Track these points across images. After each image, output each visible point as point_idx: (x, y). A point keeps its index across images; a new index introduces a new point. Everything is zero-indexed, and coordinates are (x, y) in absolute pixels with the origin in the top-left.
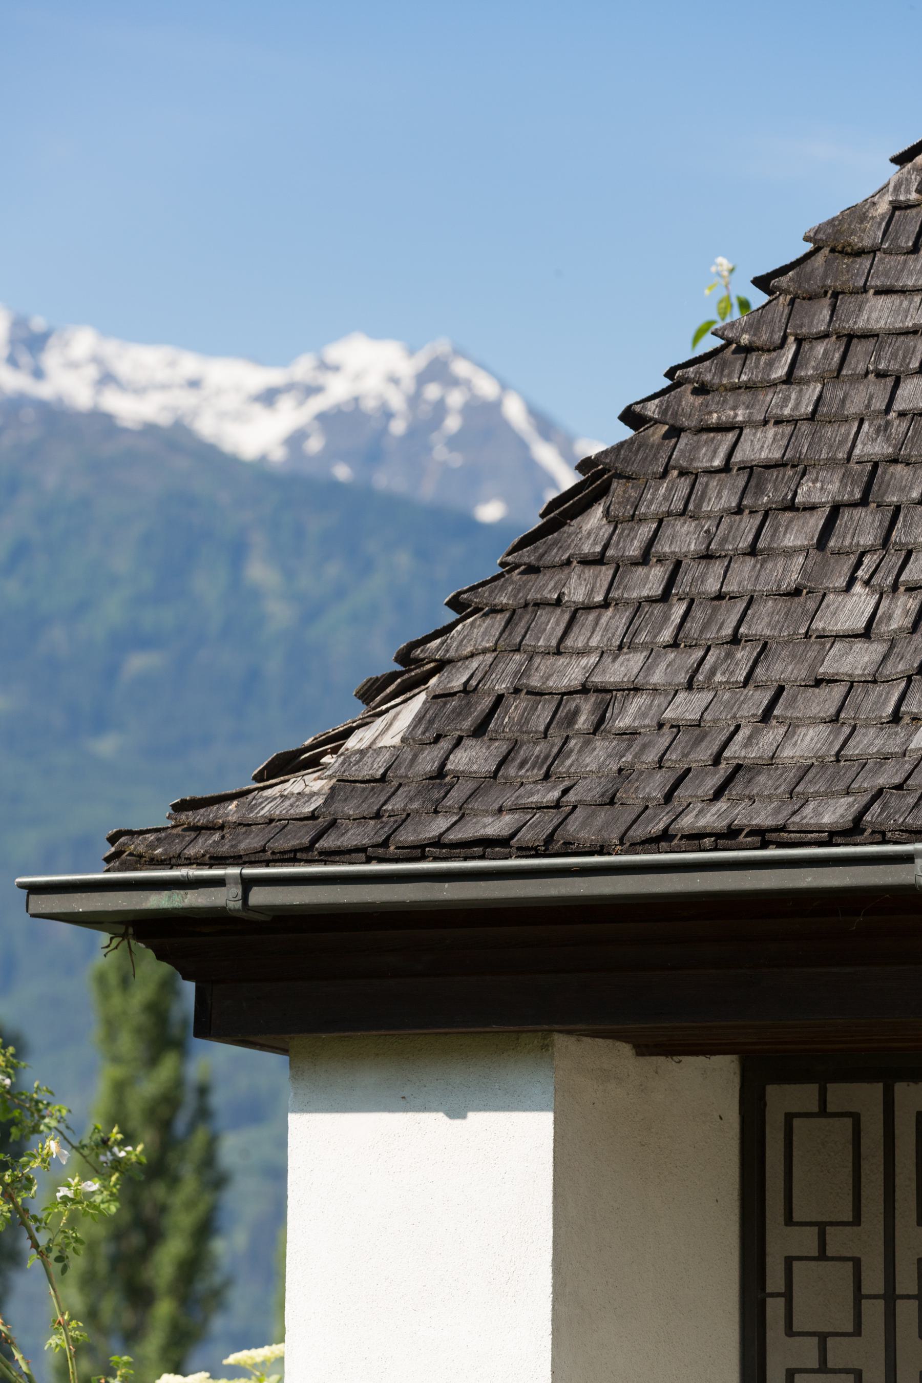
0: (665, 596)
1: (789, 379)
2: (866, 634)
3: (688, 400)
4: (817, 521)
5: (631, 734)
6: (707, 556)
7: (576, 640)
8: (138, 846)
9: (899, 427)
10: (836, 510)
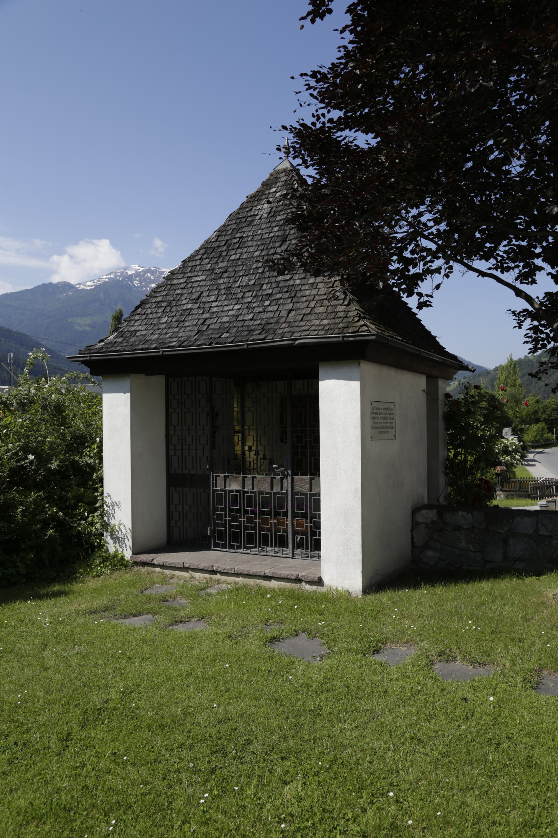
0: (145, 319)
1: (164, 290)
2: (166, 323)
3: (153, 293)
4: (163, 308)
5: (137, 336)
6: (151, 313)
7: (135, 324)
8: (81, 352)
9: (175, 296)
10: (166, 307)
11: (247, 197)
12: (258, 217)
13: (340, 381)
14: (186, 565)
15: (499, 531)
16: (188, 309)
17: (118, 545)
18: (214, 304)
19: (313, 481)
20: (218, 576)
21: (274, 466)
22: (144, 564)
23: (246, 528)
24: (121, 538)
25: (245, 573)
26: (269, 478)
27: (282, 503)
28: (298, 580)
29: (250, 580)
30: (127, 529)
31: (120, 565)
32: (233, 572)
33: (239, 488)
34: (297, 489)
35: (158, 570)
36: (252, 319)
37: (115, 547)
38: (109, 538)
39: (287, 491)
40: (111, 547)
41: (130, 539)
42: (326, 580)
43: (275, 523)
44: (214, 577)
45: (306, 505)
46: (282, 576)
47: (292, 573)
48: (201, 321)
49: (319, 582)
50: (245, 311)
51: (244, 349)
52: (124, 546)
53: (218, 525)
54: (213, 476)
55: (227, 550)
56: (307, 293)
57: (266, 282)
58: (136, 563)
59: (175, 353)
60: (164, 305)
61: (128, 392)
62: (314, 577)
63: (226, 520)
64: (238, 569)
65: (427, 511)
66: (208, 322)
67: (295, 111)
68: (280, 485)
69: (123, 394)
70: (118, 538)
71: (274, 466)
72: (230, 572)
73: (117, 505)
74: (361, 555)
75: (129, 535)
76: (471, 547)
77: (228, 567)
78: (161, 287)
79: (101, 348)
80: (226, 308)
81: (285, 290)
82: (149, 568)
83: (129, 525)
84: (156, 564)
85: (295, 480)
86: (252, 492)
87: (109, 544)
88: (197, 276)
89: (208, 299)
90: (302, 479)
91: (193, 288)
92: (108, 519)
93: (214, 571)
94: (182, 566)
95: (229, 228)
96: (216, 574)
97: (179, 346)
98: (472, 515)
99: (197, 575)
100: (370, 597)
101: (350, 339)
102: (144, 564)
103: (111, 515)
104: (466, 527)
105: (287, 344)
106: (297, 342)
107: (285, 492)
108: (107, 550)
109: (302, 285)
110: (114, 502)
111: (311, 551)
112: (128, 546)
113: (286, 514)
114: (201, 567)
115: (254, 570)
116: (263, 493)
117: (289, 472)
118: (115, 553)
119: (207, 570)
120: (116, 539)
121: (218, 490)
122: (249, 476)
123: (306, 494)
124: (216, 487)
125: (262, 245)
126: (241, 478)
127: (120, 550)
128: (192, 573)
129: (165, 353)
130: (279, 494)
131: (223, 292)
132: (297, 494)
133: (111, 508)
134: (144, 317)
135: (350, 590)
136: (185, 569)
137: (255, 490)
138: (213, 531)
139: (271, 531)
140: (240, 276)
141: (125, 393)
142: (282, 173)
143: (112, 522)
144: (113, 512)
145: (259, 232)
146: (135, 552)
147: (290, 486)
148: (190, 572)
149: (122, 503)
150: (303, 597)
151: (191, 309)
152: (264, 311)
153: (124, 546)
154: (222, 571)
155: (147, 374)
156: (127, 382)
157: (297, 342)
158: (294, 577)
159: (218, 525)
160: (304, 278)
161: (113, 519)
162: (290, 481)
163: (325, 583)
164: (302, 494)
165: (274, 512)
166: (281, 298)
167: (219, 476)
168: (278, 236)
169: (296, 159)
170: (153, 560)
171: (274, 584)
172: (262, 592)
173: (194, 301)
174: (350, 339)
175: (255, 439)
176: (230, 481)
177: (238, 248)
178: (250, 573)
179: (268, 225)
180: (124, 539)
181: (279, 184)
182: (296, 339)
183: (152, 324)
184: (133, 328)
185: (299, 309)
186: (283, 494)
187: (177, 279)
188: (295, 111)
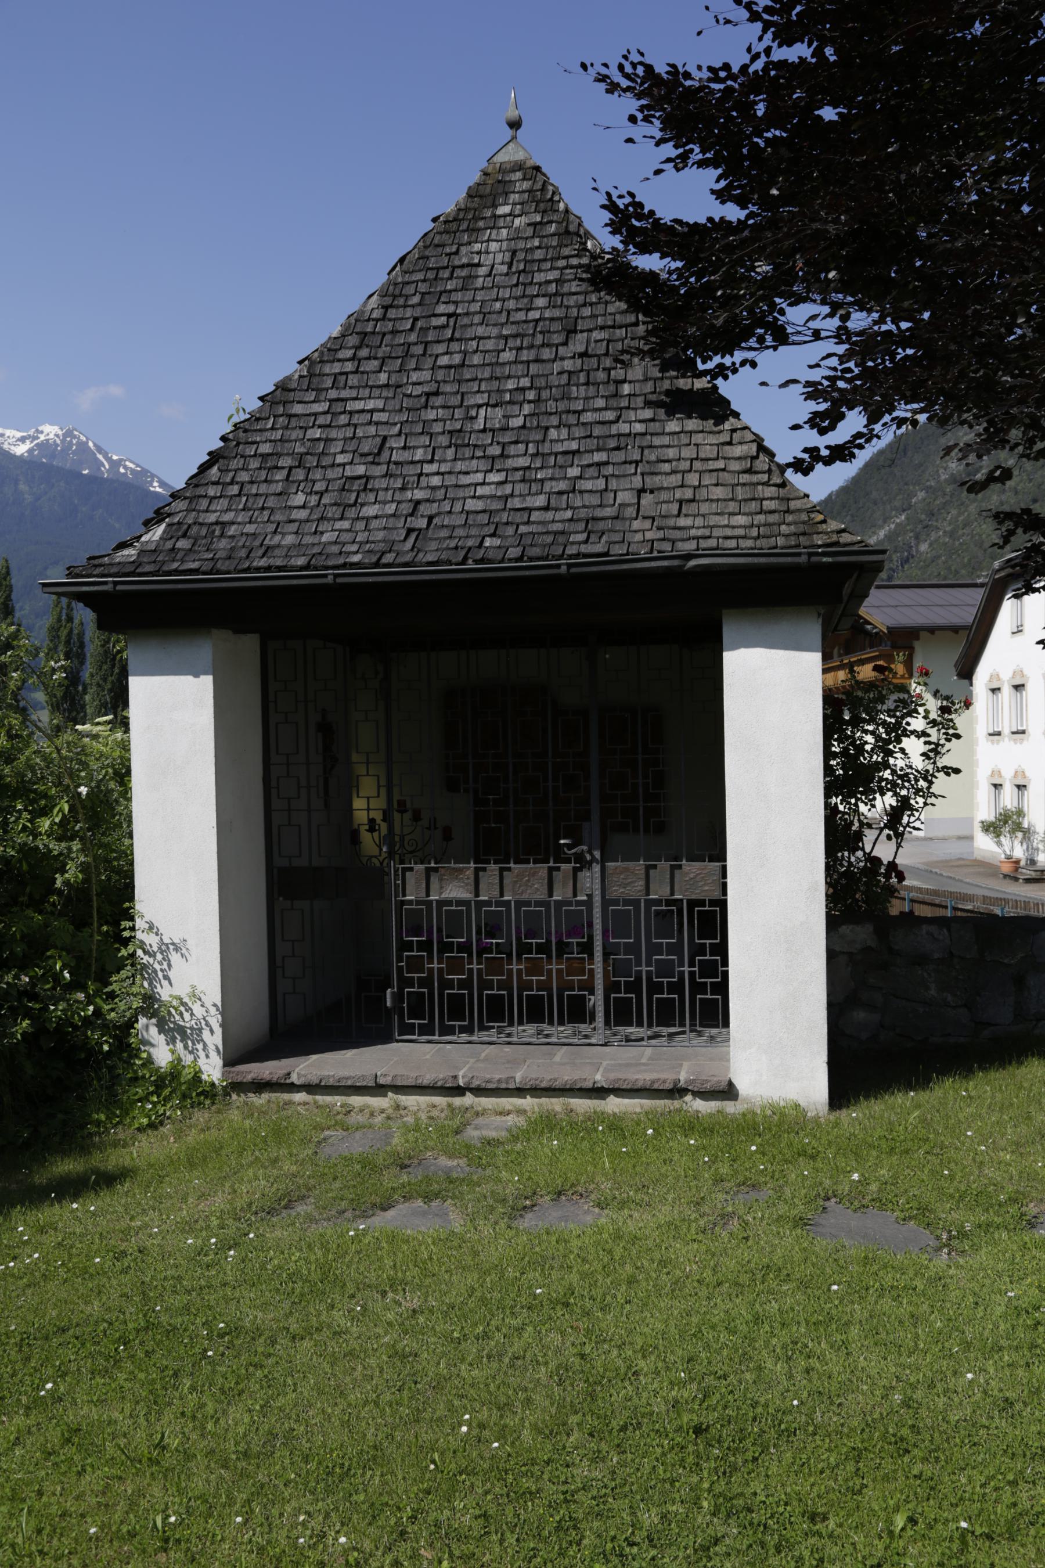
6: (252, 482)
7: (213, 508)
11: (435, 220)
12: (482, 271)
13: (773, 651)
14: (382, 1081)
15: (1006, 961)
16: (359, 477)
17: (180, 1045)
18: (428, 468)
19: (652, 872)
20: (469, 1099)
21: (562, 842)
22: (260, 1086)
23: (485, 985)
24: (192, 1028)
25: (543, 1085)
26: (542, 869)
27: (579, 924)
28: (677, 1092)
29: (554, 1100)
30: (208, 1004)
31: (198, 1095)
32: (512, 1086)
33: (465, 895)
34: (616, 891)
35: (300, 1097)
36: (546, 508)
37: (173, 1052)
38: (153, 1031)
39: (590, 896)
40: (162, 1054)
41: (218, 1031)
42: (744, 1085)
43: (559, 971)
44: (457, 1101)
45: (590, 925)
46: (639, 1085)
47: (663, 1076)
48: (405, 508)
49: (729, 1092)
50: (520, 488)
51: (559, 575)
52: (200, 1047)
53: (410, 983)
54: (396, 871)
55: (436, 1038)
56: (671, 453)
57: (555, 423)
58: (238, 1087)
59: (370, 579)
60: (286, 462)
61: (206, 673)
62: (719, 1082)
63: (431, 970)
64: (523, 1078)
65: (851, 927)
66: (425, 509)
67: (699, 33)
68: (424, 885)
69: (190, 678)
70: (181, 1030)
71: (562, 842)
72: (504, 1086)
73: (177, 949)
74: (826, 1026)
75: (215, 1021)
76: (950, 998)
77: (497, 1077)
78: (258, 419)
79: (137, 563)
80: (465, 480)
81: (612, 443)
82: (274, 1096)
83: (213, 994)
84: (297, 1082)
85: (608, 871)
86: (499, 904)
87: (153, 1045)
88: (356, 399)
89: (406, 456)
90: (627, 869)
91: (356, 426)
92: (150, 984)
93: (459, 1088)
94: (372, 1084)
95: (410, 290)
96: (463, 1095)
97: (377, 565)
98: (949, 931)
99: (411, 1101)
100: (852, 1115)
101: (825, 559)
102: (260, 1086)
103: (160, 974)
104: (936, 956)
105: (667, 567)
106: (693, 563)
107: (585, 898)
108: (149, 1061)
109: (652, 434)
110: (166, 940)
111: (650, 1026)
112: (211, 1048)
113: (587, 948)
114: (427, 1079)
115: (567, 1076)
116: (528, 903)
117: (597, 854)
118: (174, 1067)
119: (442, 1088)
120: (173, 1032)
121: (410, 902)
122: (493, 868)
123: (636, 903)
124: (404, 895)
125: (515, 336)
126: (470, 873)
127: (188, 1059)
128: (395, 1097)
129: (339, 580)
130: (570, 904)
131: (444, 440)
132: (615, 902)
133: (159, 957)
134: (235, 489)
135: (803, 1104)
136: (378, 1089)
137: (505, 898)
138: (398, 997)
139: (550, 990)
140: (480, 406)
141: (196, 676)
142: (513, 171)
143: (165, 993)
144: (165, 966)
145: (498, 305)
146: (230, 1061)
147: (597, 886)
148: (390, 1094)
149: (190, 944)
150: (691, 1125)
151: (367, 478)
152: (574, 491)
153: (200, 1047)
154: (483, 1085)
155: (237, 631)
156: (204, 649)
157: (693, 563)
158: (668, 1086)
159: (410, 983)
160: (653, 420)
161: (165, 983)
162: (598, 875)
163: (740, 1092)
164: (627, 902)
165: (438, 943)
166: (607, 463)
167: (411, 869)
168: (552, 319)
169: (662, 146)
170: (289, 1074)
171: (614, 1104)
172: (615, 1125)
173: (370, 459)
174: (825, 559)
175: (383, 782)
176: (441, 880)
177: (451, 339)
178: (557, 1084)
179: (518, 292)
180: (200, 1030)
181: (514, 197)
182: (689, 557)
183: (263, 508)
184: (212, 518)
185: (662, 488)
186: (580, 903)
187: (299, 402)
188: (699, 33)
